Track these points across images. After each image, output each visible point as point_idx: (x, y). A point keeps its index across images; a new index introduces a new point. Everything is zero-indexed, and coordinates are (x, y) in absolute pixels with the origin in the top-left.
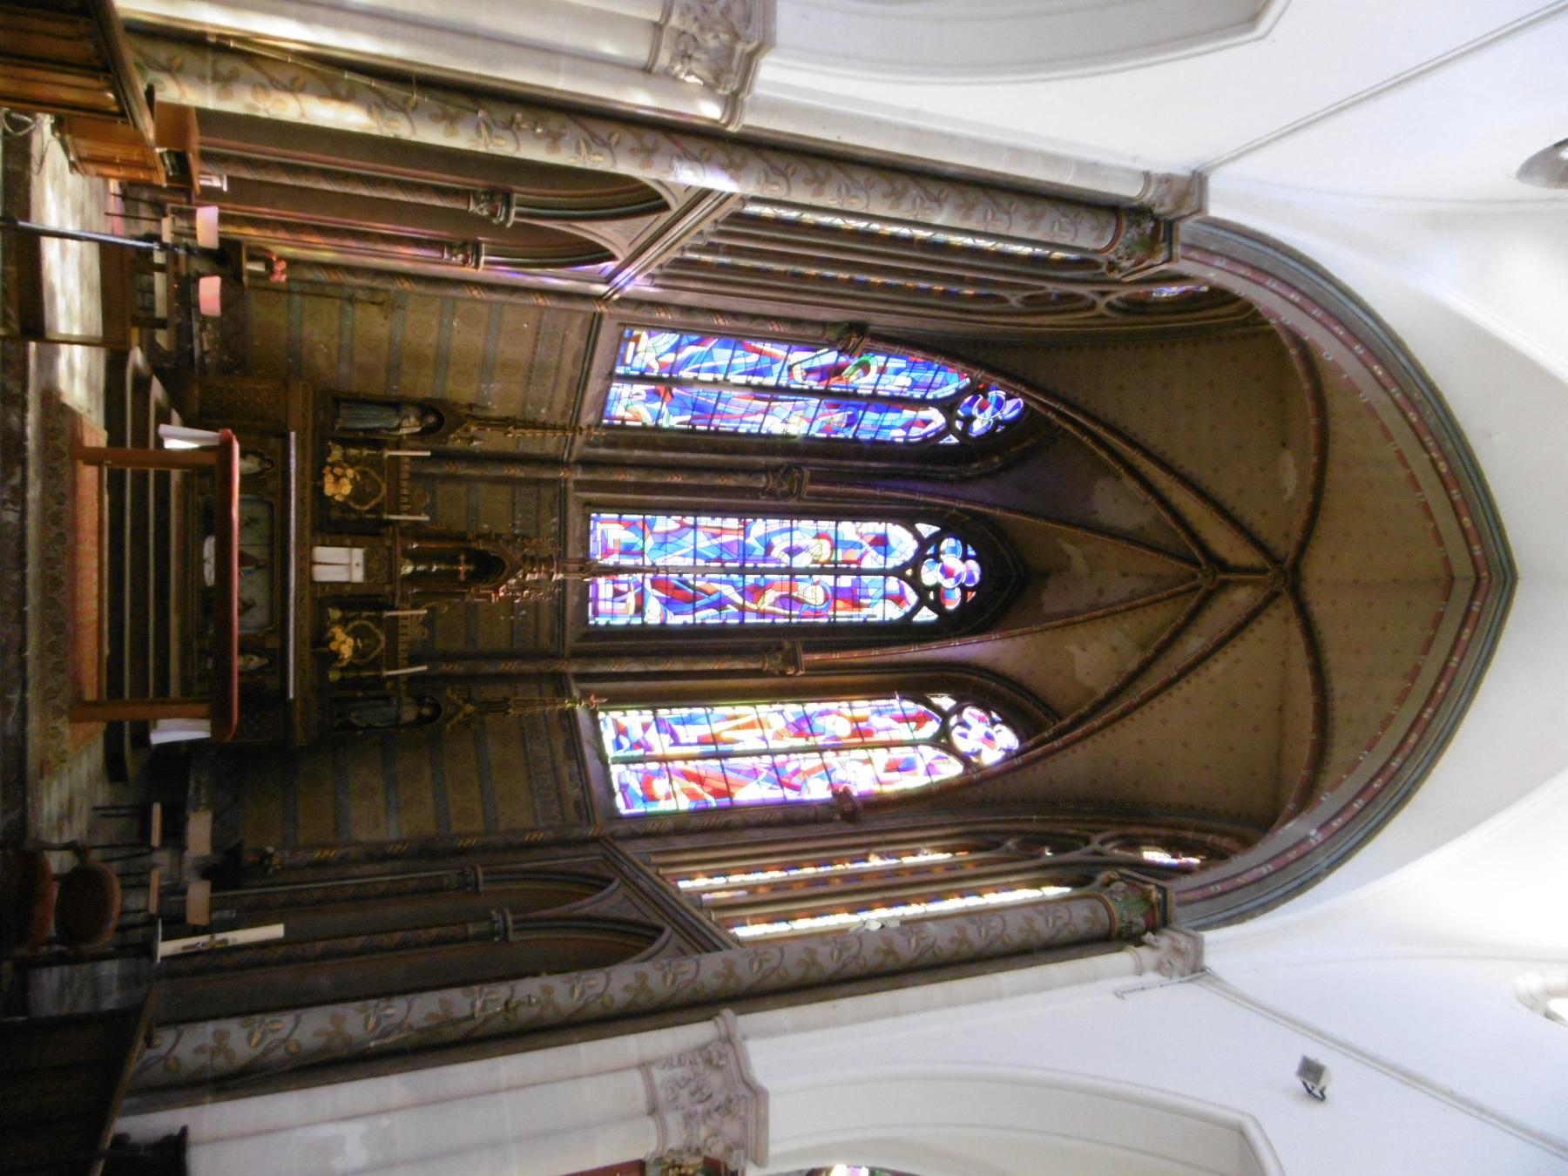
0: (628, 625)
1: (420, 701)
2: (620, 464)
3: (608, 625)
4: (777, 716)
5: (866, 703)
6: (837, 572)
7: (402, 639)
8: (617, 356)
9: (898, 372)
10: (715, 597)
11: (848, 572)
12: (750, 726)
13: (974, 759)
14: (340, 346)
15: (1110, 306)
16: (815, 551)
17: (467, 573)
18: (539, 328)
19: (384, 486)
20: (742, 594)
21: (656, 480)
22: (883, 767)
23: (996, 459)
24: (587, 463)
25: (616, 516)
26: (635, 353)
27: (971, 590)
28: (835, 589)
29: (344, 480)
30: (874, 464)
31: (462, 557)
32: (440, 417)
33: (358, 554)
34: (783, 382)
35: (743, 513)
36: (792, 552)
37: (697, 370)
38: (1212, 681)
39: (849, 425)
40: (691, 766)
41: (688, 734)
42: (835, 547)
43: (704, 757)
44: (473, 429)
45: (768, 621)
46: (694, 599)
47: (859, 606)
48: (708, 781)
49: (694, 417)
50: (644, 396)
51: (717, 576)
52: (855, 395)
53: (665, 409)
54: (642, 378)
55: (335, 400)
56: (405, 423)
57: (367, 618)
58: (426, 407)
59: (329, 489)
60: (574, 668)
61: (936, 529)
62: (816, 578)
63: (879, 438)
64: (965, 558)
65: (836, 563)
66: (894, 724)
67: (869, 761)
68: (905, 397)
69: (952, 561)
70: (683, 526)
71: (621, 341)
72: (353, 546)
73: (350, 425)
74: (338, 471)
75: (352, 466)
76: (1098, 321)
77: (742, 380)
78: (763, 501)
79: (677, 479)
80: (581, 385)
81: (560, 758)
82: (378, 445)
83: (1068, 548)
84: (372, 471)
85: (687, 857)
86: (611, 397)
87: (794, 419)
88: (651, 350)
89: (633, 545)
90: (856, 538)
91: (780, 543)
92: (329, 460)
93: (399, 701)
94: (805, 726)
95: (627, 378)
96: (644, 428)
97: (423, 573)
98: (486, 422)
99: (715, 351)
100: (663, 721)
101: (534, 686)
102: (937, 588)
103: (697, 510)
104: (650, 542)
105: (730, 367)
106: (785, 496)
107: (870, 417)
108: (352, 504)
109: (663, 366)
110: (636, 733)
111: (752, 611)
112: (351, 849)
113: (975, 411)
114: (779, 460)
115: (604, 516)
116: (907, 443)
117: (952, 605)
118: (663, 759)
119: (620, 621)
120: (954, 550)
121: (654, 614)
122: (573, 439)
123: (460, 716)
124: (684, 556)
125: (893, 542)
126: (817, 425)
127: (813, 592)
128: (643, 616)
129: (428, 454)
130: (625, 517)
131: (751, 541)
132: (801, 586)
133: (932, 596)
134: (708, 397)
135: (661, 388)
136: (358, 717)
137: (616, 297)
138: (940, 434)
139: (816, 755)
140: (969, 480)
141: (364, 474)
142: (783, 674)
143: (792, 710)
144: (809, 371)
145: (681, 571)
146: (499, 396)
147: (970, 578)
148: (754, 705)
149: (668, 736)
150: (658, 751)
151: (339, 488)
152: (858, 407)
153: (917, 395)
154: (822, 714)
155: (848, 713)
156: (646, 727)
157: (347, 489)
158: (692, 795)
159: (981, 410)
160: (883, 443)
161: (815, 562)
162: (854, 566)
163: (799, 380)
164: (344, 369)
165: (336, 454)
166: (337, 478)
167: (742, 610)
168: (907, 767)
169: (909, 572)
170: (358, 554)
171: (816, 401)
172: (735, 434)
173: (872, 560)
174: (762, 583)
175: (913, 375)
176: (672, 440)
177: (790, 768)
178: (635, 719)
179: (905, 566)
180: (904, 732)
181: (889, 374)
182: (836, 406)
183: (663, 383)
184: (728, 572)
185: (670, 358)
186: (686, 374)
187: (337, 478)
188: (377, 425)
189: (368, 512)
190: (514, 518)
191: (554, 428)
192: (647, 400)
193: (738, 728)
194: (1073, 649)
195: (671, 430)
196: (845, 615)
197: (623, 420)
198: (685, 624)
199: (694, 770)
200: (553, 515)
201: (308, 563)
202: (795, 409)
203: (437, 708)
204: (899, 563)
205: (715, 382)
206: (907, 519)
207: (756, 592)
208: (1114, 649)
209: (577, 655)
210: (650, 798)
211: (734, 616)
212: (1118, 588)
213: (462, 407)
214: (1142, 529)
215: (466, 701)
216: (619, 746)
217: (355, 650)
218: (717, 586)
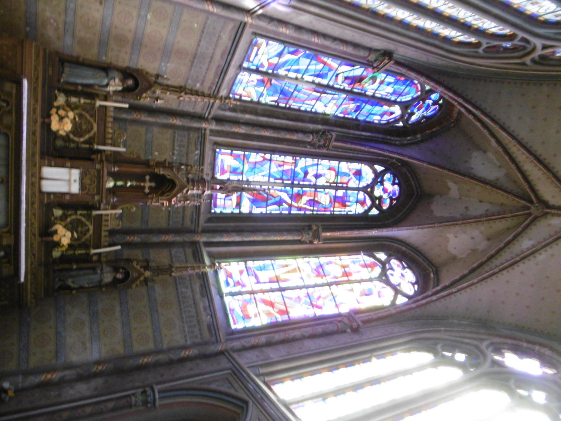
0: (232, 213)
1: (116, 270)
3: (221, 213)
4: (306, 265)
6: (337, 188)
7: (104, 228)
8: (246, 57)
9: (389, 84)
10: (277, 199)
11: (342, 188)
12: (294, 271)
13: (398, 288)
14: (65, 23)
15: (533, 61)
16: (328, 176)
17: (150, 188)
18: (204, 27)
19: (95, 126)
20: (291, 198)
21: (256, 133)
22: (359, 294)
23: (419, 136)
24: (219, 120)
25: (229, 151)
26: (256, 55)
27: (394, 199)
28: (336, 197)
29: (66, 120)
30: (364, 133)
31: (148, 178)
32: (136, 81)
33: (76, 173)
34: (331, 83)
39: (356, 111)
41: (264, 276)
42: (337, 175)
43: (272, 290)
44: (158, 92)
45: (302, 212)
46: (267, 200)
47: (345, 206)
48: (276, 305)
49: (279, 98)
50: (256, 82)
51: (279, 188)
52: (364, 95)
53: (265, 92)
54: (257, 71)
55: (64, 61)
56: (112, 82)
57: (81, 215)
58: (127, 73)
59: (55, 125)
60: (203, 239)
62: (327, 191)
63: (368, 120)
64: (393, 184)
65: (337, 183)
66: (361, 269)
67: (352, 290)
68: (389, 97)
69: (388, 185)
71: (251, 45)
72: (72, 167)
73: (72, 80)
74: (62, 112)
75: (72, 110)
76: (520, 67)
77: (310, 79)
78: (308, 149)
79: (267, 133)
80: (223, 72)
81: (198, 296)
82: (92, 96)
83: (450, 184)
84: (91, 116)
85: (279, 367)
86: (237, 81)
88: (266, 53)
90: (347, 171)
91: (312, 171)
92: (56, 104)
93: (102, 270)
94: (321, 270)
95: (249, 70)
96: (252, 102)
97: (121, 187)
98: (167, 88)
99: (301, 59)
101: (181, 250)
102: (380, 198)
103: (273, 151)
105: (306, 71)
106: (319, 147)
108: (71, 136)
109: (270, 65)
111: (295, 207)
112: (67, 372)
113: (415, 110)
114: (320, 127)
117: (385, 207)
118: (252, 293)
119: (228, 211)
120: (389, 180)
121: (246, 208)
123: (142, 278)
124: (263, 176)
125: (363, 174)
127: (324, 198)
128: (240, 208)
129: (127, 106)
130: (235, 152)
131: (298, 169)
132: (319, 194)
133: (377, 202)
134: (289, 87)
135: (266, 78)
136: (73, 282)
137: (260, 12)
138: (396, 121)
139: (328, 287)
140: (403, 145)
141: (81, 116)
142: (311, 242)
143: (314, 261)
144: (346, 78)
145: (261, 184)
146: (173, 71)
147: (394, 194)
148: (295, 259)
149: (253, 277)
150: (248, 288)
151: (62, 125)
152: (364, 102)
153: (393, 98)
154: (328, 264)
155: (340, 263)
156: (241, 272)
157: (68, 126)
158: (269, 314)
160: (369, 122)
161: (327, 182)
162: (345, 185)
163: (341, 83)
164: (68, 41)
165: (61, 100)
166: (61, 118)
167: (290, 206)
168: (368, 294)
169: (369, 190)
170: (76, 173)
171: (344, 96)
172: (299, 110)
173: (354, 183)
174: (301, 192)
175: (396, 87)
177: (316, 296)
178: (234, 267)
179: (368, 186)
180: (366, 273)
183: (268, 76)
184: (286, 185)
185: (275, 61)
186: (282, 72)
187: (61, 118)
188: (91, 82)
189: (84, 142)
190: (173, 149)
191: (203, 95)
192: (256, 86)
193: (289, 272)
194: (451, 236)
195: (266, 104)
196: (338, 210)
197: (241, 96)
198: (262, 213)
199: (268, 299)
200: (197, 149)
201: (36, 178)
202: (332, 99)
203: (127, 275)
204: (365, 185)
205: (296, 79)
206: (371, 162)
207: (297, 197)
208: (473, 238)
209: (205, 231)
210: (246, 317)
211: (286, 209)
212: (479, 209)
213: (151, 75)
214: (498, 179)
215: (146, 268)
216: (228, 284)
217: (72, 238)
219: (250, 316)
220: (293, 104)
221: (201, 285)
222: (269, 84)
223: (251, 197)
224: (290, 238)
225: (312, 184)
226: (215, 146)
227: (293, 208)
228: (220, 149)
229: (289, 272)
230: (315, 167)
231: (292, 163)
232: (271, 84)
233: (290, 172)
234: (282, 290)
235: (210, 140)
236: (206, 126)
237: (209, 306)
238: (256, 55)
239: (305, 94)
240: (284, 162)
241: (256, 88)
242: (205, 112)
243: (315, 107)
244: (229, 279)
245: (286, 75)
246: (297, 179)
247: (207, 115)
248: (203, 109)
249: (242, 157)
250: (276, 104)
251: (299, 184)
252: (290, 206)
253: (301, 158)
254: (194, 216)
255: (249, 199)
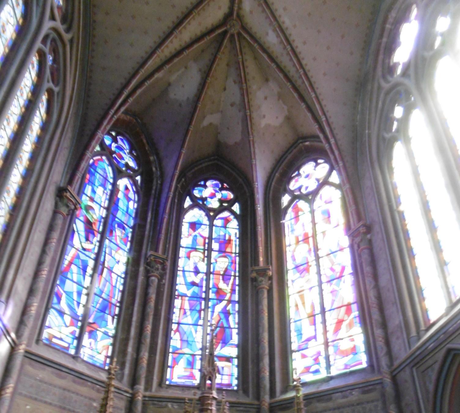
0: (238, 366)
2: (136, 362)
3: (237, 379)
4: (295, 284)
5: (287, 238)
6: (210, 250)
8: (63, 351)
9: (94, 192)
10: (222, 316)
11: (210, 244)
12: (302, 297)
13: (321, 181)
16: (197, 260)
18: (31, 398)
20: (221, 301)
21: (148, 340)
22: (328, 225)
26: (61, 339)
27: (223, 185)
34: (93, 256)
35: (172, 297)
36: (197, 272)
37: (79, 303)
38: (295, 26)
39: (124, 228)
40: (331, 328)
41: (308, 331)
42: (195, 249)
43: (324, 322)
45: (237, 288)
46: (223, 328)
47: (230, 241)
48: (340, 317)
49: (109, 314)
52: (106, 219)
53: (103, 330)
54: (79, 339)
60: (267, 399)
61: (188, 199)
62: (213, 261)
63: (133, 215)
64: (205, 186)
65: (204, 250)
66: (300, 223)
67: (324, 233)
68: (108, 191)
69: (206, 193)
70: (177, 330)
71: (50, 345)
76: (75, 45)
77: (88, 279)
78: (166, 281)
79: (149, 328)
80: (80, 376)
81: (330, 405)
83: (205, 123)
86: (91, 361)
87: (117, 257)
88: (59, 328)
89: (188, 361)
90: (191, 238)
91: (191, 277)
95: (78, 348)
96: (113, 345)
99: (65, 290)
100: (299, 346)
102: (221, 201)
103: (169, 321)
104: (186, 350)
105: (79, 284)
106: (164, 269)
107: (120, 215)
109: (72, 324)
110: (309, 361)
111: (231, 297)
113: (123, 162)
114: (142, 269)
115: (168, 376)
116: (138, 202)
117: (231, 196)
119: (235, 371)
120: (200, 191)
121: (232, 351)
122: (116, 388)
124: (196, 331)
125: (194, 220)
126: (123, 246)
127: (221, 264)
128: (232, 358)
130: (170, 364)
131: (189, 293)
132: (217, 269)
133: (225, 205)
135: (87, 329)
137: (13, 335)
138: (135, 183)
142: (270, 278)
143: (291, 276)
144: (87, 239)
145: (205, 334)
147: (216, 185)
148: (289, 296)
149: (310, 343)
152: (113, 220)
153: (110, 187)
156: (304, 356)
158: (350, 325)
159: (122, 158)
160: (136, 213)
161: (203, 260)
162: (207, 241)
163: (93, 245)
167: (230, 301)
168: (328, 215)
169: (212, 214)
172: (123, 292)
173: (204, 231)
174: (215, 290)
176: (123, 328)
177: (330, 273)
179: (208, 215)
181: (94, 199)
182: (111, 232)
183: (85, 327)
184: (207, 307)
185: (68, 319)
186: (80, 311)
191: (106, 399)
192: (95, 340)
193: (303, 303)
194: (264, 122)
195: (117, 329)
196: (234, 247)
197: (107, 357)
198: (238, 334)
199: (334, 326)
200: (166, 406)
202: (110, 254)
204: (206, 218)
205: (88, 295)
206: (181, 212)
207: (220, 294)
208: (266, 98)
209: (258, 397)
210: (354, 351)
211: (234, 307)
212: (233, 92)
214: (200, 70)
216: (317, 371)
218: (216, 314)
219: (352, 346)
220: (116, 298)
221: (319, 401)
222: (94, 326)
223: (220, 345)
224: (265, 302)
225: (205, 277)
226: (163, 385)
227: (233, 299)
228: (167, 380)
229: (303, 303)
230: (186, 273)
231: (182, 299)
232: (94, 323)
233: (192, 302)
234: (323, 311)
235: (156, 391)
236: (141, 395)
237: (341, 392)
238: (61, 339)
239: (104, 285)
240: (180, 309)
241: (99, 339)
242: (125, 397)
243: (119, 274)
244: (312, 369)
245: (84, 306)
246: (199, 294)
247: (128, 395)
248: (122, 399)
249: (176, 355)
250: (116, 317)
251: (205, 292)
252: (230, 301)
253: (177, 290)
254: (241, 408)
255: (222, 348)
